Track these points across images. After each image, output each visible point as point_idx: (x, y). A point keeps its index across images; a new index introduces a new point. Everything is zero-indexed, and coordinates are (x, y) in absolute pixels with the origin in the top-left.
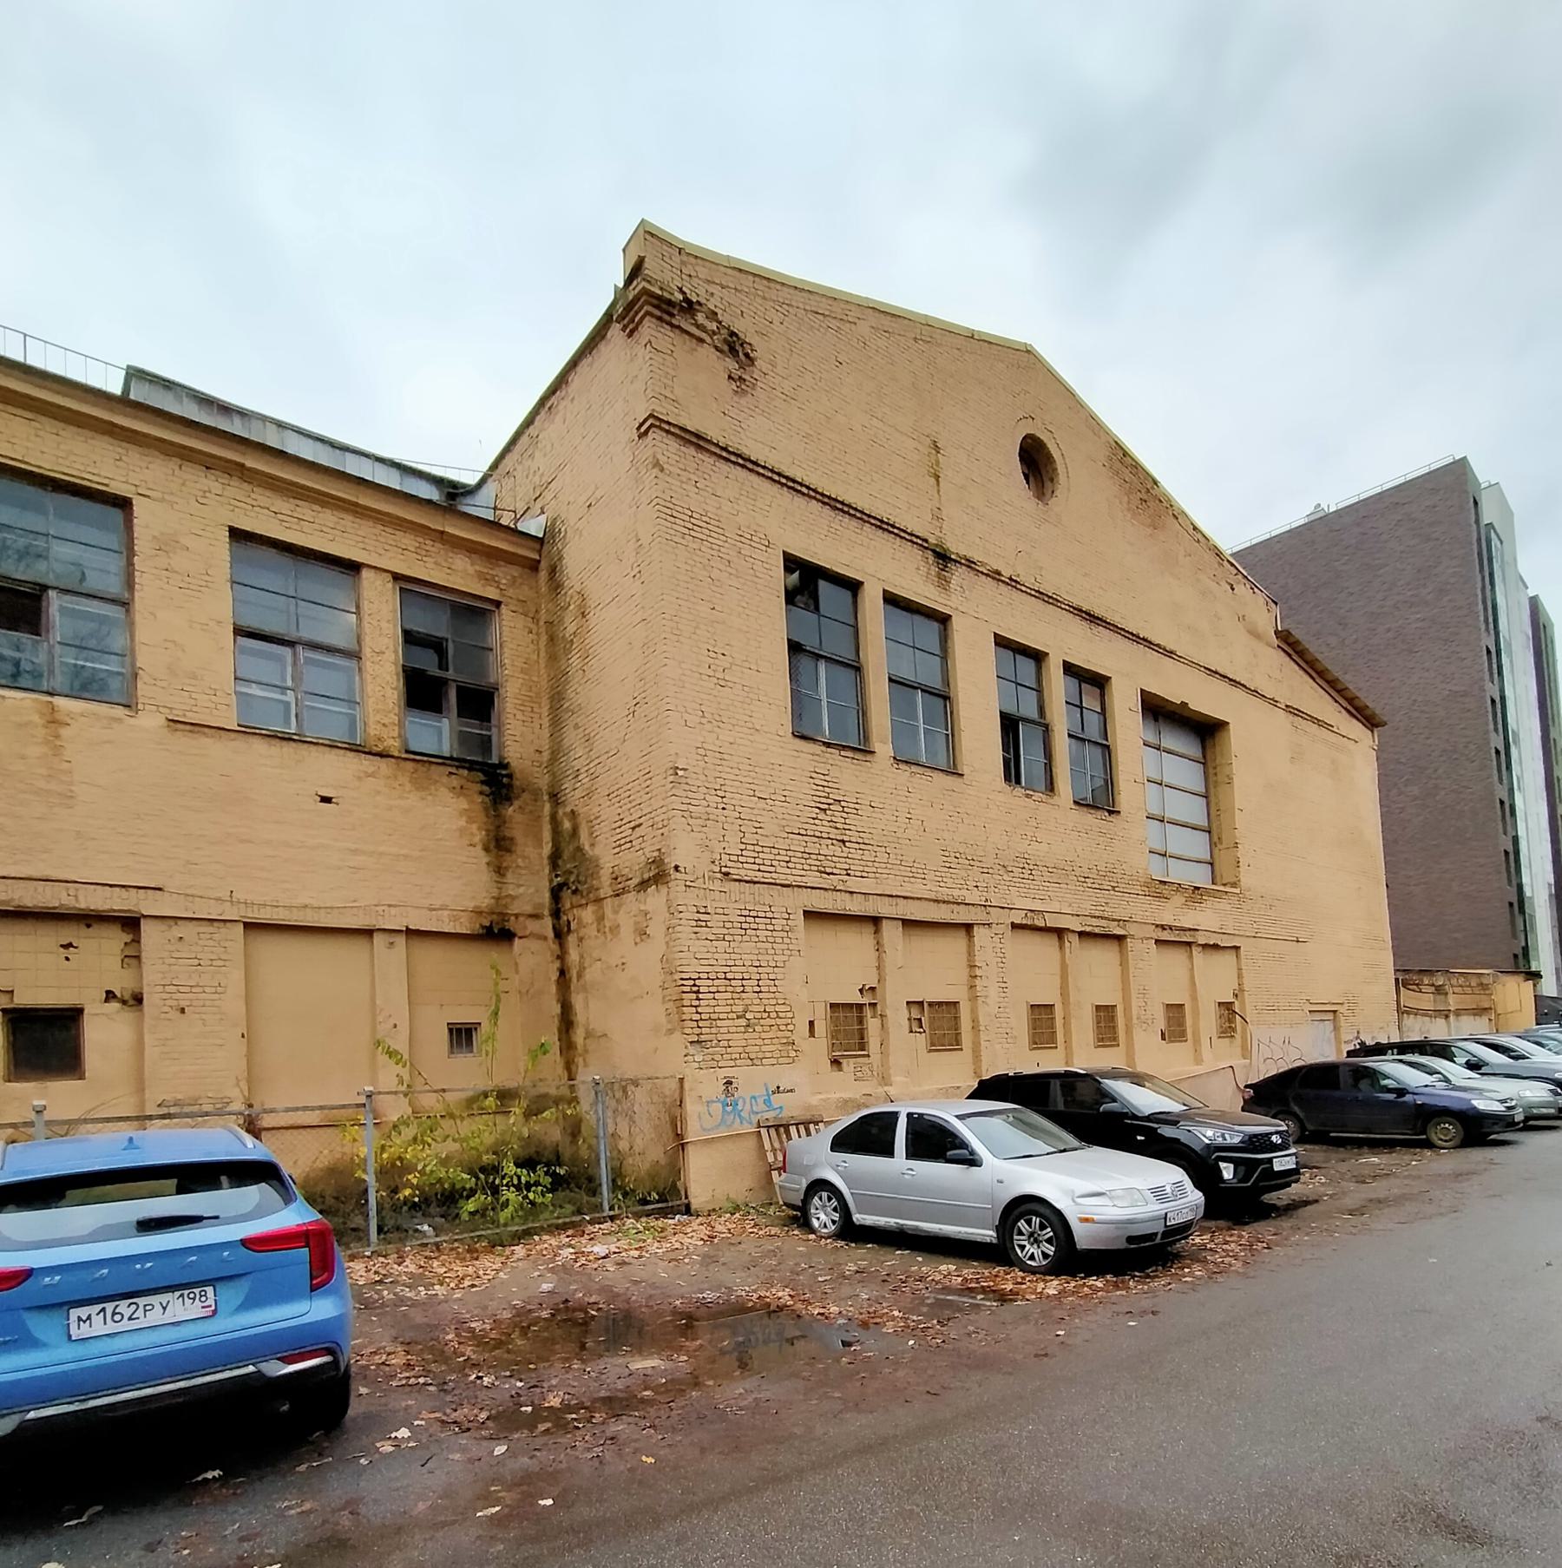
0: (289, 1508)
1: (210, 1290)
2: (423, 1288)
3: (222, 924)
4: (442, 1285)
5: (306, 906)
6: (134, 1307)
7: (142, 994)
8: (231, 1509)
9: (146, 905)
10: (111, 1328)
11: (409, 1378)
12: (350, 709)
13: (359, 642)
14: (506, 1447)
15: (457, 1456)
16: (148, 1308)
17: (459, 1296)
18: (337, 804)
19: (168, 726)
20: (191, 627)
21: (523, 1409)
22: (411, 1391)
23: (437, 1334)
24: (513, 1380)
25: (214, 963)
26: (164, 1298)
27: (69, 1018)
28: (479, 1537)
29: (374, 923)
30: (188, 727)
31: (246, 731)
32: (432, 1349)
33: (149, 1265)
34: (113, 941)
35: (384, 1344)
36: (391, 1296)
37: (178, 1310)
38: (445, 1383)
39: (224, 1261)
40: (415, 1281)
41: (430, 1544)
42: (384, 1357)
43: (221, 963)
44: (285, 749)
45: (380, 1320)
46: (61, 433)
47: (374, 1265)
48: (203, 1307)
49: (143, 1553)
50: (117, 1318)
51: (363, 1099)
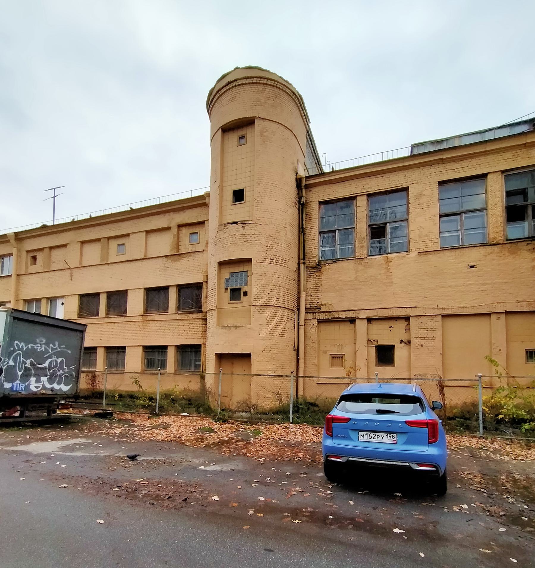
0: (415, 515)
1: (395, 435)
2: (499, 455)
3: (434, 316)
4: (508, 456)
5: (464, 307)
6: (374, 435)
7: (410, 340)
8: (399, 507)
9: (411, 312)
10: (368, 440)
11: (478, 487)
12: (483, 230)
13: (487, 204)
14: (506, 530)
15: (482, 524)
16: (378, 436)
17: (514, 462)
18: (477, 267)
19: (419, 254)
20: (426, 220)
21: (523, 518)
22: (476, 493)
23: (498, 475)
24: (523, 505)
25: (432, 330)
26: (383, 434)
27: (391, 348)
28: (475, 558)
29: (491, 310)
30: (424, 253)
31: (444, 249)
32: (493, 480)
33: (378, 423)
34: (402, 324)
35: (474, 472)
36: (484, 455)
37: (386, 439)
38: (492, 494)
39: (399, 427)
40: (496, 452)
41: (456, 550)
42: (472, 477)
43: (434, 329)
44: (457, 252)
45: (476, 463)
46: (390, 176)
47: (481, 441)
48: (393, 440)
49: (372, 509)
50: (370, 437)
51: (477, 378)
